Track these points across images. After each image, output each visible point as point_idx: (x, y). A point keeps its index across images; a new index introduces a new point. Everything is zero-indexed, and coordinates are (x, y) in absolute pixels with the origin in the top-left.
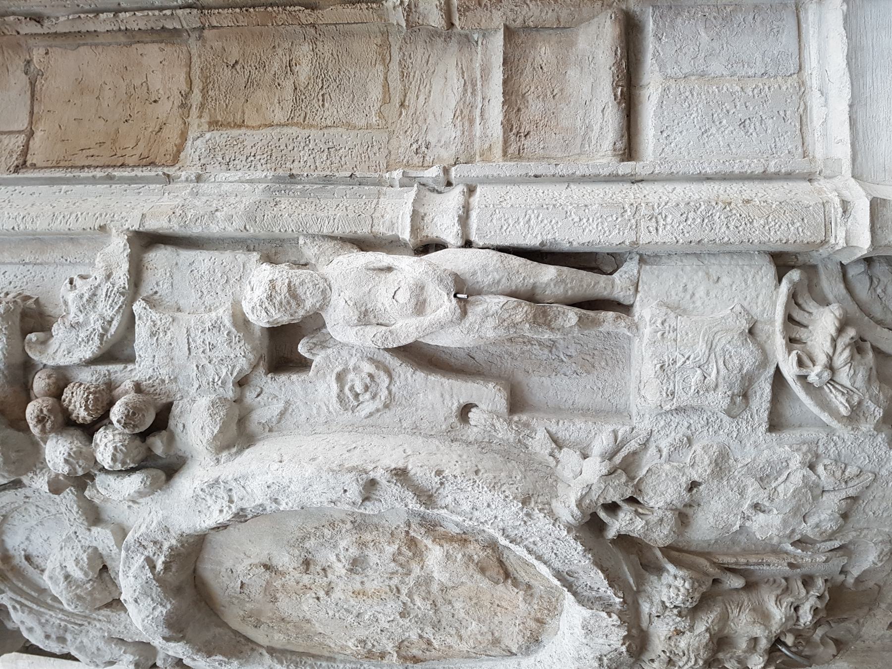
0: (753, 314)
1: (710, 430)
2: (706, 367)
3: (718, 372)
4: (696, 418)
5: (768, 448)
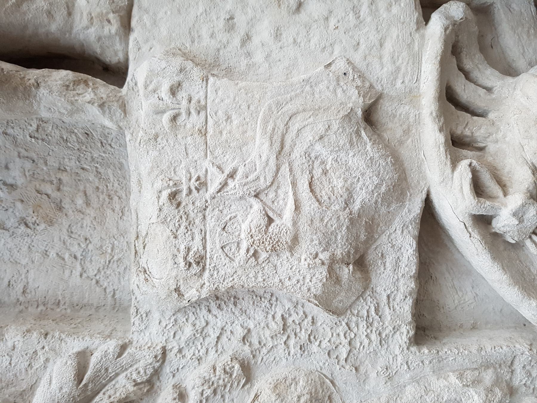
0: (373, 80)
1: (292, 342)
2: (272, 195)
3: (297, 207)
4: (259, 316)
5: (416, 380)
